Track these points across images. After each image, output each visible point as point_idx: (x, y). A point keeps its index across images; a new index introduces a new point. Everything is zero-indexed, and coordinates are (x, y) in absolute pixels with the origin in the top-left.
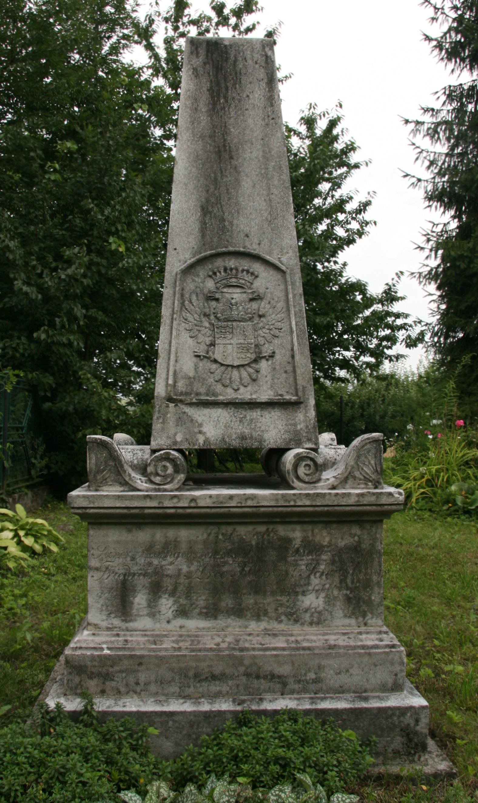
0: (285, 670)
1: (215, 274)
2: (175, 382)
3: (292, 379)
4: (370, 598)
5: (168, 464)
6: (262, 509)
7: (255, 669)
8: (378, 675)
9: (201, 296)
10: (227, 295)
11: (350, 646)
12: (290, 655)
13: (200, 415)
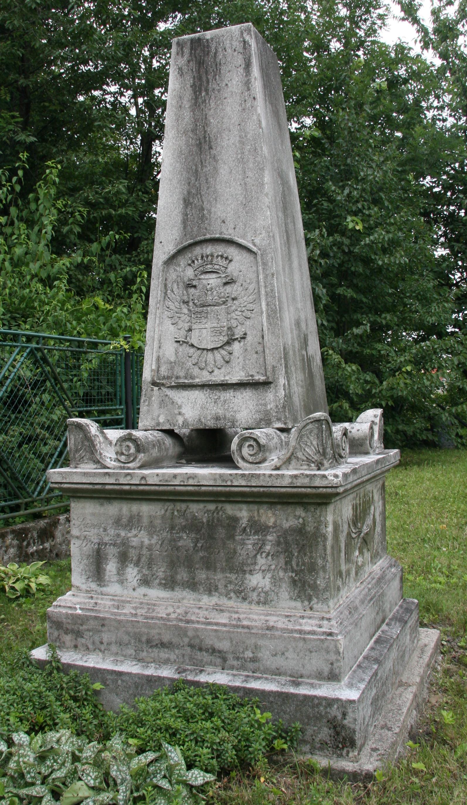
0: (224, 645)
1: (193, 262)
2: (159, 367)
3: (262, 359)
4: (315, 583)
5: (131, 444)
6: (203, 488)
7: (197, 641)
8: (314, 662)
9: (181, 284)
11: (288, 629)
12: (229, 632)
13: (181, 397)
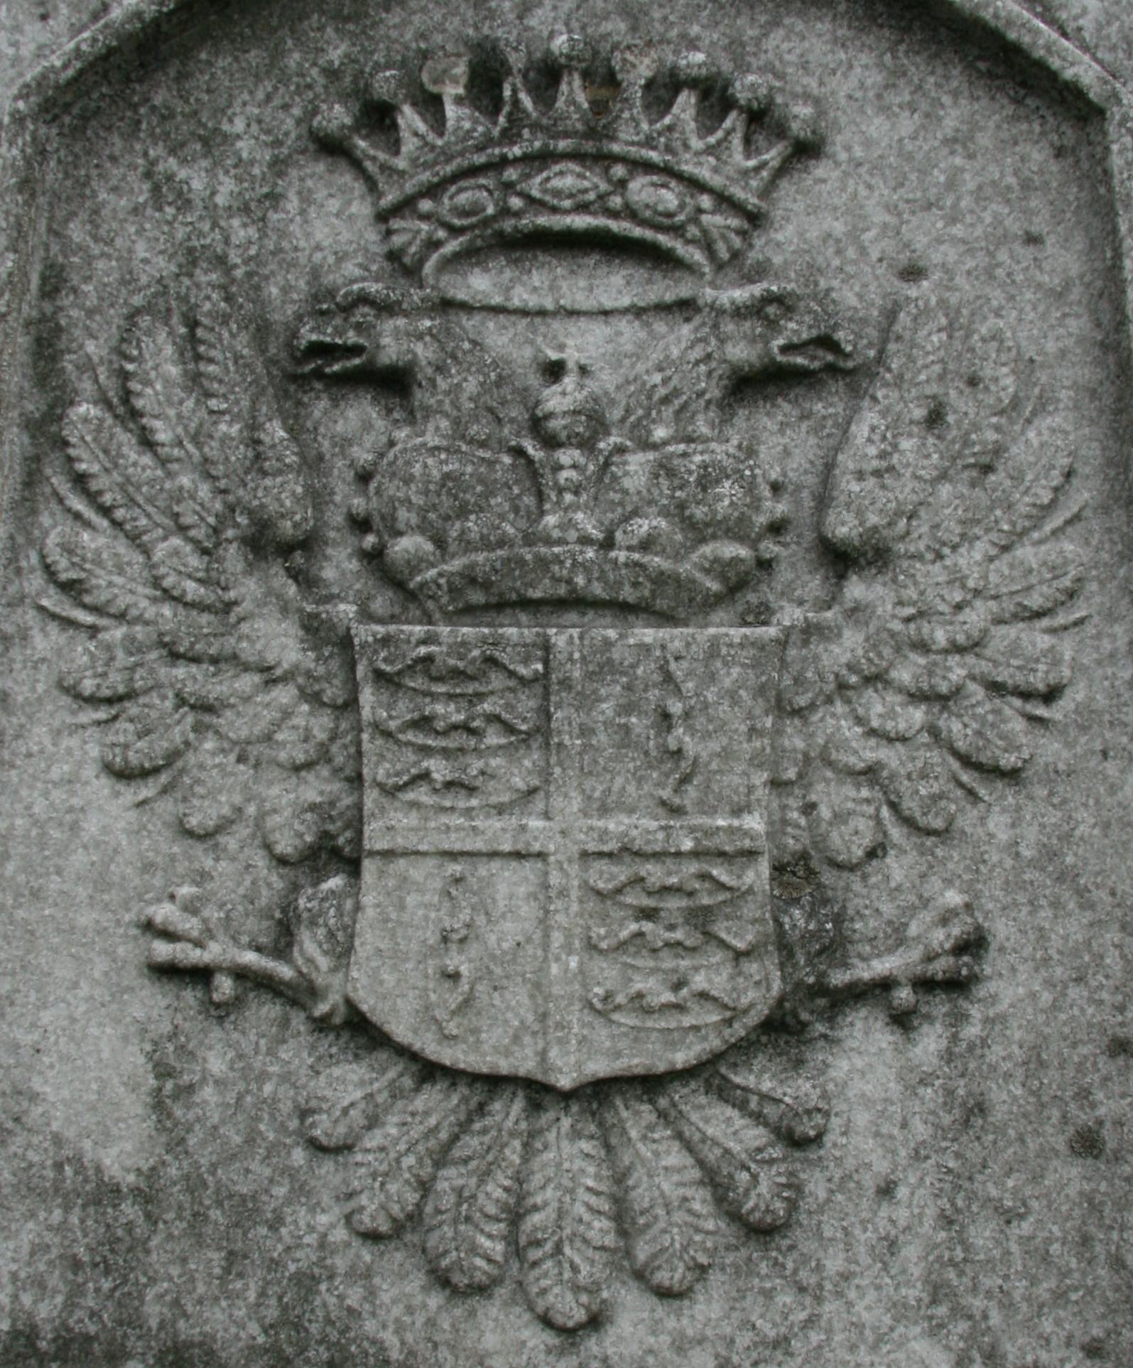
1: (378, 117)
10: (499, 338)
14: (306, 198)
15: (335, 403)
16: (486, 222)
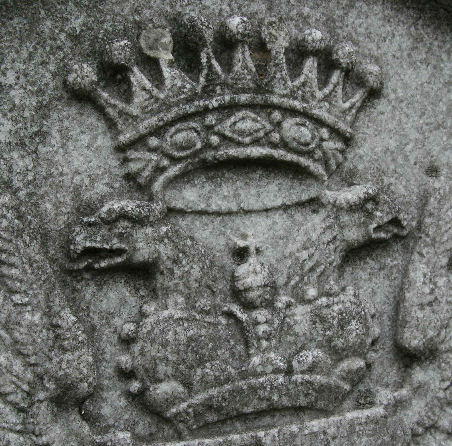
1: (115, 75)
10: (205, 233)
14: (65, 136)
15: (100, 287)
16: (196, 154)
